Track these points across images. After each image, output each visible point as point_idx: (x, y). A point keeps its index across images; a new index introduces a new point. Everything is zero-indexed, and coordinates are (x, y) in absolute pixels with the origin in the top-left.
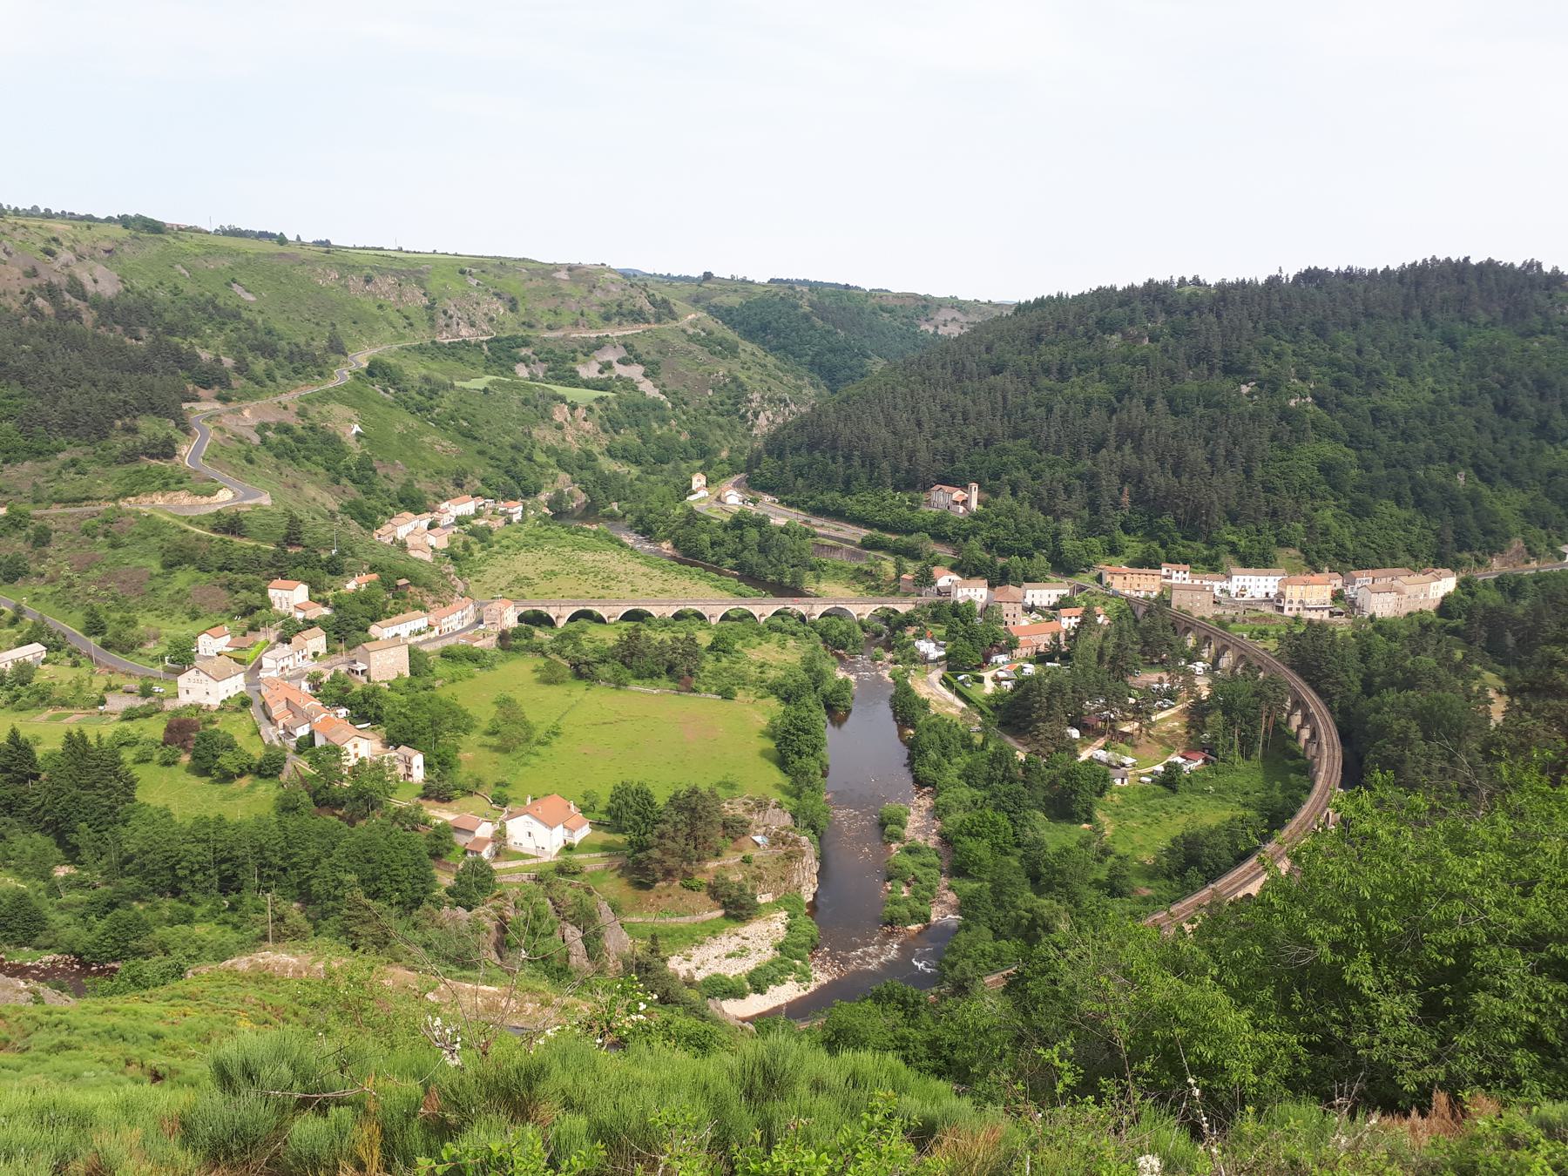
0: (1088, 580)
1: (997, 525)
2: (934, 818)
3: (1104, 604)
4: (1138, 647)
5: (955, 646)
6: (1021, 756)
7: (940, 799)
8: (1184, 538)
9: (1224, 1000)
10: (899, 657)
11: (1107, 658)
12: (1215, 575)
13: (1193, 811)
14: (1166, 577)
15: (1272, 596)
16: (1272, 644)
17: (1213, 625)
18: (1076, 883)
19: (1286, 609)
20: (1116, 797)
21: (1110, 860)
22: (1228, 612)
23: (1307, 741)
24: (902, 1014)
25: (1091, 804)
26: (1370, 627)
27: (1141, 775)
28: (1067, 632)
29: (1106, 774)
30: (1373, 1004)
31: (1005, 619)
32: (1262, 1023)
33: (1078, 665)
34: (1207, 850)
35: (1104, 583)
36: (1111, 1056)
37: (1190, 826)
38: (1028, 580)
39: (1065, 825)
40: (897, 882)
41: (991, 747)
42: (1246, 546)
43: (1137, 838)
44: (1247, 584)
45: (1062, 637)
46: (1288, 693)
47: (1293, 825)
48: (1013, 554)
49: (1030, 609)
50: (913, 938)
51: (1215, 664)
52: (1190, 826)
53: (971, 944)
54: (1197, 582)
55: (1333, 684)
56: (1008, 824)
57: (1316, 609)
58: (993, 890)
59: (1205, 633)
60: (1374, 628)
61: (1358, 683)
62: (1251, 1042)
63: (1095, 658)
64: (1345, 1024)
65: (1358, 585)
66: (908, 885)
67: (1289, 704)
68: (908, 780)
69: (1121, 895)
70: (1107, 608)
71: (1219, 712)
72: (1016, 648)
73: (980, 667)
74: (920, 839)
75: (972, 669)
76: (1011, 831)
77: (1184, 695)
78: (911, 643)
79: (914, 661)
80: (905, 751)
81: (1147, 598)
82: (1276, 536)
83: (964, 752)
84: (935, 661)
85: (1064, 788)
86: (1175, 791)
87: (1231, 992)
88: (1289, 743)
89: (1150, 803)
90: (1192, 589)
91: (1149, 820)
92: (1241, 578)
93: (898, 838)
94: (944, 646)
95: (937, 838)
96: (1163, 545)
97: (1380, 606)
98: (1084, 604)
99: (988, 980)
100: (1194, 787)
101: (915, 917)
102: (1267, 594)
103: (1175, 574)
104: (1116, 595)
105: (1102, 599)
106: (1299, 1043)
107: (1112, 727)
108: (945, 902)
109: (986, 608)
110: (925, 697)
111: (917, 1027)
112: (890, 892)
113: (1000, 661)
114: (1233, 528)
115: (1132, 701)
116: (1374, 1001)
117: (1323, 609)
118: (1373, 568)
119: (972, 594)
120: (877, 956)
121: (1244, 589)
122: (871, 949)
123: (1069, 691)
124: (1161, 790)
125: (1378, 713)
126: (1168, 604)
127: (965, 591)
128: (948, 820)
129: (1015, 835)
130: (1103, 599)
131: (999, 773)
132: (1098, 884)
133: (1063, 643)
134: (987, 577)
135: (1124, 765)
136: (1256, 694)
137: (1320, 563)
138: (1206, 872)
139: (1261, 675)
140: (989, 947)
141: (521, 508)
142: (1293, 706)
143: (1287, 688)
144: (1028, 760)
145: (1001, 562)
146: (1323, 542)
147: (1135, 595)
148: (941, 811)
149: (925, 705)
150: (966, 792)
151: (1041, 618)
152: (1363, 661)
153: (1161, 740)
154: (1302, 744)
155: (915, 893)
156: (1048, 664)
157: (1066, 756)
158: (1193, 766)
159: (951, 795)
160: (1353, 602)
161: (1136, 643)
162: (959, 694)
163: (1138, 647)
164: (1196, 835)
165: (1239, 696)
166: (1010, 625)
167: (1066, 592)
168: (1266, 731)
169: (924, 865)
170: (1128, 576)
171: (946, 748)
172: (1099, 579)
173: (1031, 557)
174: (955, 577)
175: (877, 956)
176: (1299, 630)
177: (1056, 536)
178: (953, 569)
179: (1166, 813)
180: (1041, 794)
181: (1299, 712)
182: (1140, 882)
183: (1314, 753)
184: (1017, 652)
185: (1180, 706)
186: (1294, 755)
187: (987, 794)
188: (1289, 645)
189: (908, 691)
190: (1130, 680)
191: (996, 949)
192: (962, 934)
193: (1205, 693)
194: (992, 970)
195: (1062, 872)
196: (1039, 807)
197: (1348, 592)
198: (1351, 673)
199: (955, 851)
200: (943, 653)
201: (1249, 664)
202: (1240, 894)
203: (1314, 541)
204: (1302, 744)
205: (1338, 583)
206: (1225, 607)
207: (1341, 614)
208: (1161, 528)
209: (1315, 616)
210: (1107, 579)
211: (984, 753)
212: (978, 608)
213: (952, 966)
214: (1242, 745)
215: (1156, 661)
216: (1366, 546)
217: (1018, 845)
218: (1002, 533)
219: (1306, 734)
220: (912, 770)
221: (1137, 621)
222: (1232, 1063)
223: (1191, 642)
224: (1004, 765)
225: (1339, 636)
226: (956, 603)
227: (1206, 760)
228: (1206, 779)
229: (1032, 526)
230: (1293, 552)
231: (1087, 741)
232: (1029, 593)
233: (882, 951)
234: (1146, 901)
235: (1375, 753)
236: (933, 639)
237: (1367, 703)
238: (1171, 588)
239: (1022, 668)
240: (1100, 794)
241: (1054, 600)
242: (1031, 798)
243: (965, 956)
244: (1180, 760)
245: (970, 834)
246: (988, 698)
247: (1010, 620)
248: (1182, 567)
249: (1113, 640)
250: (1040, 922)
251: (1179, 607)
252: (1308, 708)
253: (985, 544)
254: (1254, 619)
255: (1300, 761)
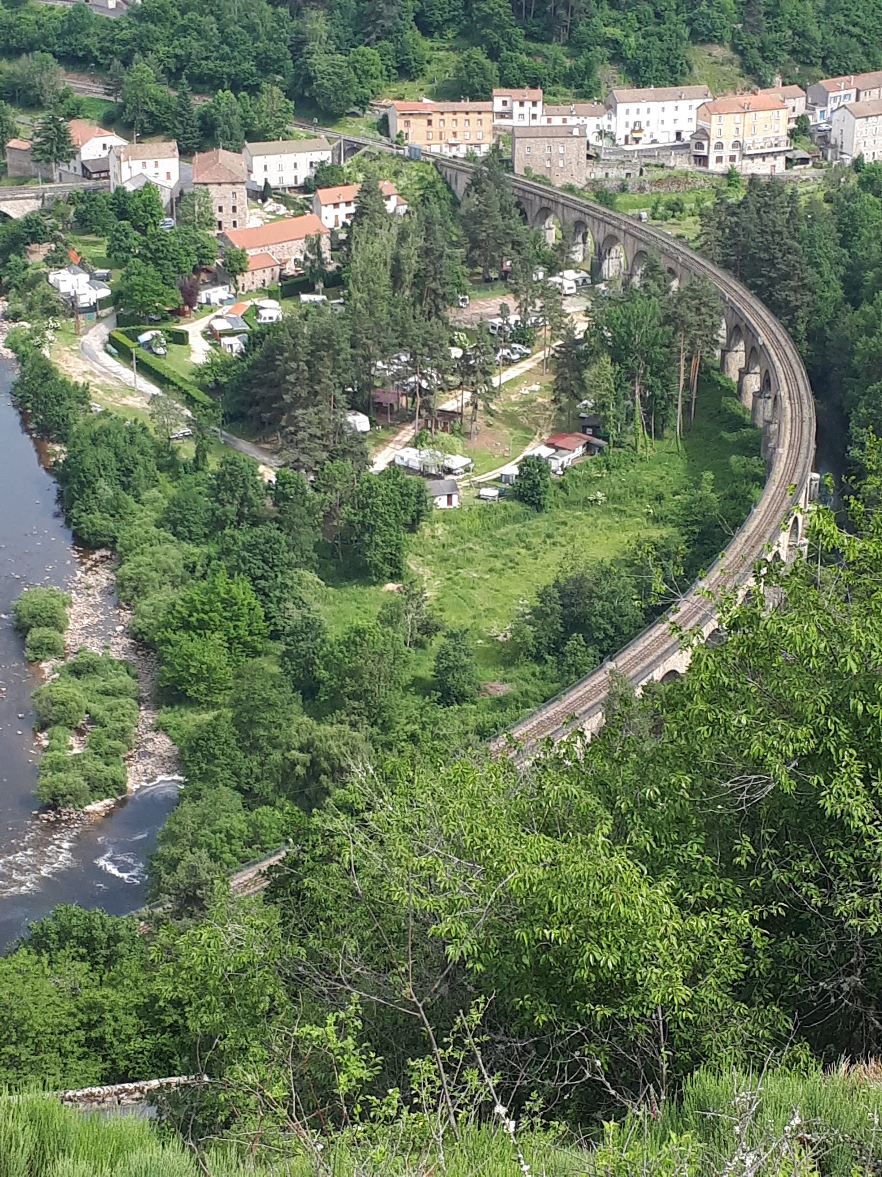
0: (364, 130)
1: (184, 30)
2: (118, 606)
3: (396, 174)
4: (461, 252)
5: (127, 277)
6: (268, 474)
7: (126, 569)
8: (529, 36)
9: (633, 872)
10: (21, 307)
11: (408, 278)
12: (587, 106)
13: (573, 538)
14: (502, 115)
15: (686, 137)
16: (690, 227)
17: (589, 200)
18: (381, 689)
19: (712, 159)
20: (440, 529)
21: (438, 641)
22: (614, 173)
23: (757, 396)
24: (86, 966)
25: (398, 549)
26: (854, 179)
27: (480, 485)
28: (333, 233)
29: (420, 492)
30: (868, 843)
31: (218, 216)
32: (692, 899)
33: (357, 295)
34: (598, 605)
35: (393, 133)
36: (452, 990)
37: (567, 565)
38: (253, 136)
39: (354, 589)
40: (58, 730)
41: (213, 463)
42: (639, 46)
43: (479, 596)
44: (643, 118)
45: (325, 244)
46: (721, 314)
47: (728, 558)
48: (220, 86)
49: (262, 194)
50: (99, 827)
51: (595, 272)
52: (567, 565)
53: (204, 820)
54: (557, 121)
55: (795, 290)
56: (251, 598)
57: (763, 156)
58: (236, 722)
59: (575, 216)
60: (861, 183)
61: (837, 284)
62: (678, 934)
63: (386, 279)
64: (823, 883)
65: (832, 105)
66: (80, 732)
67: (723, 332)
68: (63, 542)
69: (461, 698)
70: (402, 182)
71: (606, 359)
72: (242, 271)
73: (178, 313)
74: (94, 647)
75: (165, 319)
76: (261, 612)
77: (545, 333)
78: (41, 277)
79: (51, 312)
80: (50, 484)
81: (471, 157)
82: (689, 22)
83: (162, 477)
84: (92, 309)
85: (350, 523)
86: (539, 507)
87: (640, 855)
88: (727, 402)
89: (498, 533)
90: (549, 134)
91: (498, 564)
92: (633, 107)
93: (52, 650)
94: (107, 278)
95: (126, 641)
96: (493, 54)
97: (870, 141)
98: (360, 177)
99: (237, 880)
100: (573, 498)
101: (97, 788)
102: (678, 135)
103: (517, 109)
104: (415, 155)
105: (391, 165)
106: (752, 920)
107: (426, 405)
108: (150, 755)
109: (180, 198)
110: (81, 380)
111: (113, 983)
112: (46, 749)
113: (214, 299)
114: (614, 14)
115: (456, 352)
116: (870, 837)
117: (774, 155)
118: (856, 71)
119: (150, 171)
120: (35, 869)
121: (637, 128)
122: (19, 857)
123: (346, 345)
124: (516, 507)
125: (871, 335)
126: (508, 165)
127: (137, 165)
128: (144, 606)
129: (268, 617)
130: (394, 165)
131: (231, 509)
132: (420, 686)
133: (327, 254)
134: (176, 136)
135: (450, 471)
136: (668, 320)
137: (766, 69)
138: (599, 642)
139: (675, 284)
140: (238, 822)
141: (404, 398)
142: (729, 338)
143: (719, 305)
144: (282, 480)
145: (199, 103)
146: (770, 29)
147: (449, 153)
148: (129, 592)
149: (82, 396)
150: (174, 552)
151: (283, 210)
152: (843, 244)
153: (511, 419)
154: (748, 401)
155: (95, 747)
156: (305, 297)
157: (348, 465)
158: (567, 459)
159: (147, 559)
160: (824, 139)
161: (453, 244)
162: (145, 369)
163: (461, 252)
164: (579, 581)
165: (638, 326)
166: (227, 226)
167: (326, 156)
168: (687, 386)
169: (106, 693)
170: (435, 118)
171: (128, 472)
172: (383, 126)
173: (254, 90)
174: (114, 140)
175: (35, 869)
176: (735, 196)
177: (298, 46)
178: (109, 122)
179: (528, 548)
180: (309, 537)
181: (741, 346)
182: (490, 673)
183: (768, 415)
184: (246, 280)
185: (541, 355)
186: (737, 423)
187: (211, 549)
188: (720, 226)
189: (47, 372)
190: (451, 314)
191: (251, 824)
192: (187, 807)
193: (581, 327)
194: (245, 861)
195: (354, 674)
196: (307, 563)
197: (816, 119)
198: (826, 267)
199: (161, 661)
200: (105, 292)
201: (653, 268)
202: (658, 674)
203: (754, 29)
204: (748, 401)
205: (799, 104)
206: (608, 164)
207: (804, 161)
208: (486, 19)
209: (761, 168)
210: (398, 125)
211: (200, 475)
212: (165, 198)
213: (173, 865)
214: (648, 413)
215: (494, 275)
216: (843, 32)
217: (275, 636)
218: (195, 46)
219: (753, 383)
220: (68, 522)
221: (455, 203)
222: (653, 974)
223: (552, 234)
224: (239, 493)
225: (803, 201)
226: (120, 191)
227: (589, 446)
228: (591, 481)
229: (251, 29)
230: (720, 52)
231: (383, 434)
232: (258, 162)
233: (42, 858)
234: (501, 703)
235: (868, 405)
236: (82, 265)
237: (851, 318)
238: (511, 136)
239: (256, 310)
240: (412, 527)
241: (304, 173)
242: (291, 548)
243: (195, 844)
244: (545, 452)
245: (186, 626)
246: (199, 372)
247: (226, 217)
248: (528, 93)
249: (417, 242)
250: (325, 765)
251: (527, 170)
252: (755, 336)
253: (167, 71)
254: (658, 182)
255: (746, 432)
